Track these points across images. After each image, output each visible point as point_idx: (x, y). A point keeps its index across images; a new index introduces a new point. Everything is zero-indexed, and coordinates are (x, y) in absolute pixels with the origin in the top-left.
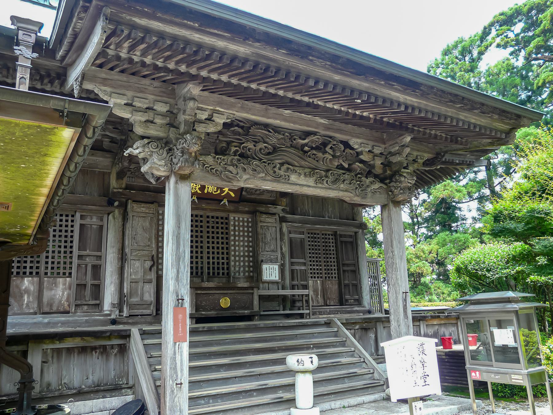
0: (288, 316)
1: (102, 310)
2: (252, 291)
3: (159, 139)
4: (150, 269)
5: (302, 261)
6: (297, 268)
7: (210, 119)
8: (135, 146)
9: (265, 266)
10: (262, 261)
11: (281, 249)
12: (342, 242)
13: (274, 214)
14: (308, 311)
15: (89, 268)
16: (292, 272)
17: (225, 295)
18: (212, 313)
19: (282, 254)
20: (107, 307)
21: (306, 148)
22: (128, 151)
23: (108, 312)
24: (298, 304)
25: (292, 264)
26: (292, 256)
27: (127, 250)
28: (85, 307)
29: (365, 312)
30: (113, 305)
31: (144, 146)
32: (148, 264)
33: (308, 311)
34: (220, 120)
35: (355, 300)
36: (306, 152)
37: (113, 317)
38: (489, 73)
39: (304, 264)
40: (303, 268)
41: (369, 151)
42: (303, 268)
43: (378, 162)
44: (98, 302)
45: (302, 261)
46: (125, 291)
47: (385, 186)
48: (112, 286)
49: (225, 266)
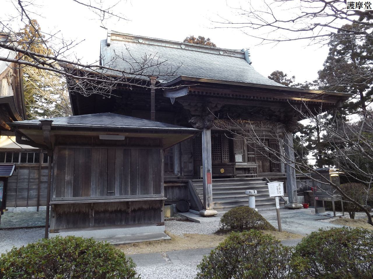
0: (247, 177)
1: (174, 173)
2: (247, 200)
3: (199, 116)
4: (191, 158)
5: (253, 153)
6: (251, 156)
7: (216, 106)
8: (192, 119)
9: (236, 156)
10: (235, 154)
11: (244, 148)
12: (271, 144)
13: (240, 133)
14: (256, 175)
15: (169, 158)
16: (248, 157)
17: (222, 168)
18: (217, 175)
19: (244, 150)
20: (176, 172)
21: (252, 113)
22: (190, 121)
23: (176, 174)
24: (251, 172)
25: (248, 154)
26: (248, 151)
27: (182, 151)
28: (168, 172)
29: (281, 175)
30: (178, 172)
31: (195, 119)
32: (190, 156)
33: (256, 175)
34: (219, 107)
35: (277, 170)
36: (252, 115)
37: (178, 176)
38: (188, 206)
39: (254, 154)
40: (253, 156)
41: (279, 111)
42: (253, 156)
43: (282, 115)
44: (172, 170)
45: (253, 153)
46: (182, 166)
47: (285, 125)
48: (177, 164)
49: (214, 152)
